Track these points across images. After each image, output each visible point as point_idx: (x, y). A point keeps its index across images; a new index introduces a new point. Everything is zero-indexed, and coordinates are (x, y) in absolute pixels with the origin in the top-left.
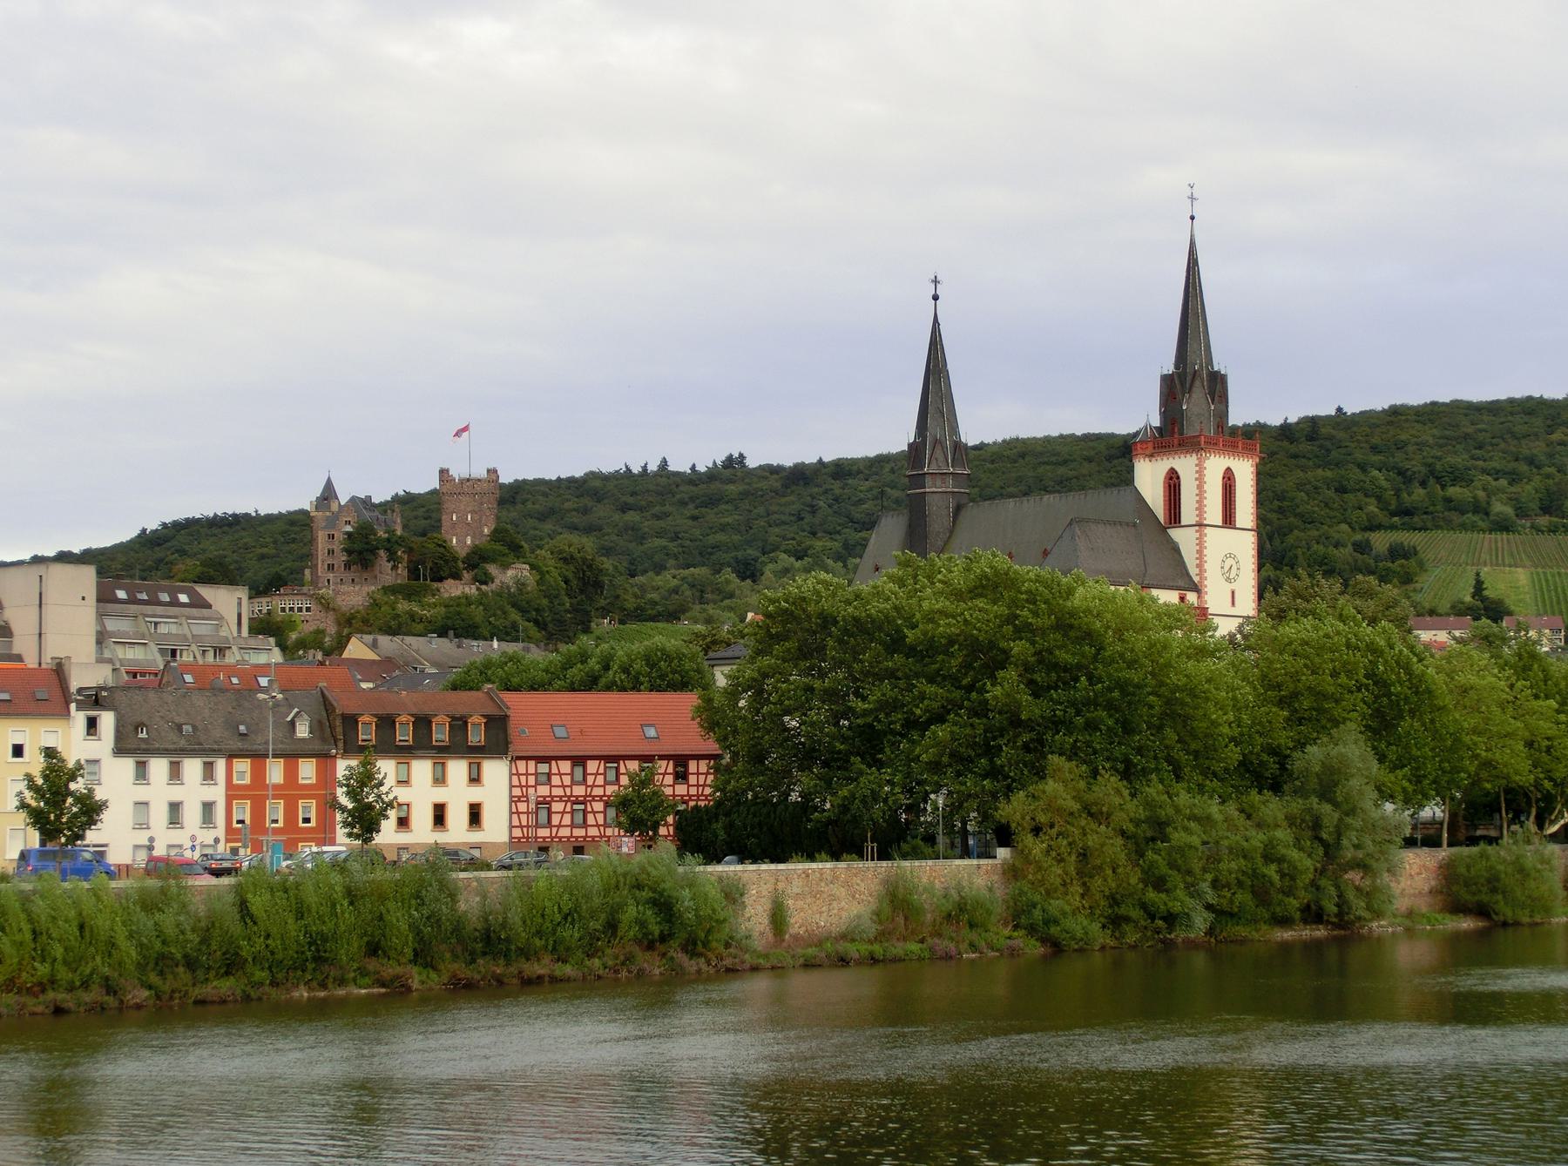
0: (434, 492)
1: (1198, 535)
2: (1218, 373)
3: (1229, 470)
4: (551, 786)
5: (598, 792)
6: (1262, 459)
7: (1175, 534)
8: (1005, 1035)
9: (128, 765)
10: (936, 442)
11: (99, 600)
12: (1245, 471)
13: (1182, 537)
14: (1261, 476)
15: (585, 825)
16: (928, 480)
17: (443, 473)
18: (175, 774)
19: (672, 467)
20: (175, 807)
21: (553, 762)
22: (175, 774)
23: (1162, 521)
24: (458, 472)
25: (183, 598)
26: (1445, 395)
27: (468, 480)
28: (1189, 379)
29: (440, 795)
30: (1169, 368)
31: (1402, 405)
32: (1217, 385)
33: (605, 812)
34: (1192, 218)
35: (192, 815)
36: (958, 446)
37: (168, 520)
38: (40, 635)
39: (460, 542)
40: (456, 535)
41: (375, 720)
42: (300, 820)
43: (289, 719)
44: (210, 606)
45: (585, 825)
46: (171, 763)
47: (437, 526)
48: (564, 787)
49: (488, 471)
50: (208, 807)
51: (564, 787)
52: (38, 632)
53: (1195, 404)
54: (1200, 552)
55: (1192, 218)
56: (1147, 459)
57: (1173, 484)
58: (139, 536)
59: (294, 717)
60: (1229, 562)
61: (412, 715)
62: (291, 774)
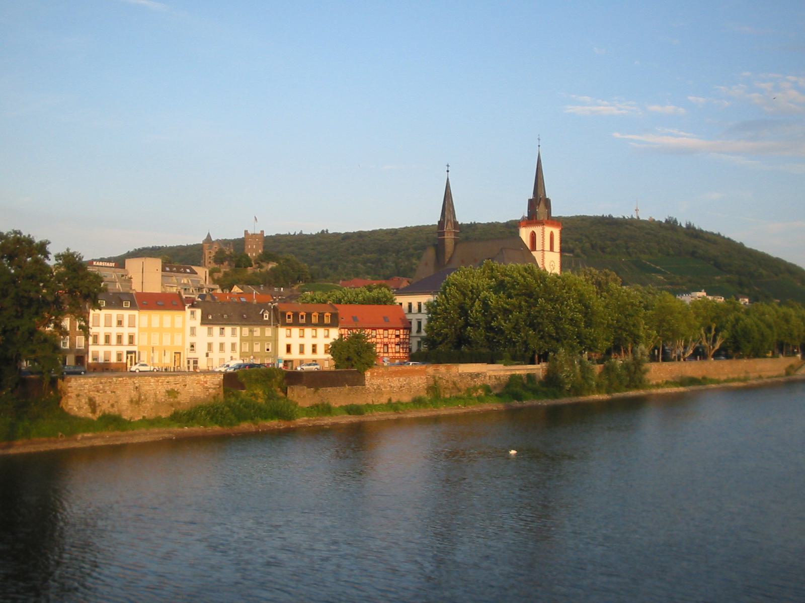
0: (243, 238)
1: (542, 254)
2: (548, 199)
3: (533, 232)
4: (377, 339)
5: (393, 341)
6: (562, 229)
7: (534, 253)
8: (389, 420)
9: (205, 328)
10: (448, 221)
11: (162, 271)
12: (556, 232)
13: (536, 254)
14: (561, 233)
15: (388, 352)
16: (446, 234)
17: (246, 232)
18: (222, 333)
19: (304, 233)
20: (222, 345)
21: (377, 330)
22: (222, 333)
23: (529, 248)
24: (250, 232)
25: (188, 271)
26: (377, 228)
27: (254, 234)
28: (539, 200)
29: (302, 341)
30: (531, 197)
31: (510, 221)
32: (547, 203)
33: (383, 348)
34: (539, 146)
35: (228, 347)
36: (456, 223)
37: (137, 248)
38: (142, 283)
39: (252, 255)
40: (250, 252)
41: (330, 314)
42: (266, 350)
43: (261, 313)
44: (196, 273)
45: (388, 352)
46: (232, 328)
47: (244, 249)
48: (381, 338)
49: (261, 231)
50: (233, 345)
51: (381, 338)
52: (141, 281)
53: (541, 210)
54: (543, 260)
55: (539, 146)
56: (605, 216)
57: (533, 236)
58: (127, 253)
59: (263, 312)
60: (552, 263)
61: (292, 312)
62: (263, 333)
